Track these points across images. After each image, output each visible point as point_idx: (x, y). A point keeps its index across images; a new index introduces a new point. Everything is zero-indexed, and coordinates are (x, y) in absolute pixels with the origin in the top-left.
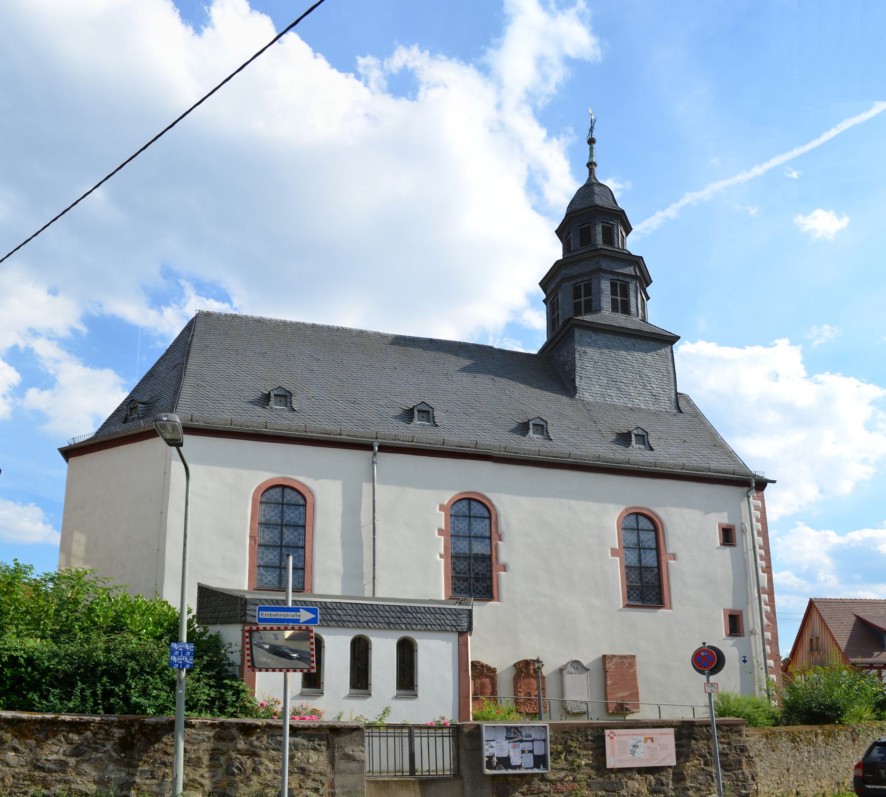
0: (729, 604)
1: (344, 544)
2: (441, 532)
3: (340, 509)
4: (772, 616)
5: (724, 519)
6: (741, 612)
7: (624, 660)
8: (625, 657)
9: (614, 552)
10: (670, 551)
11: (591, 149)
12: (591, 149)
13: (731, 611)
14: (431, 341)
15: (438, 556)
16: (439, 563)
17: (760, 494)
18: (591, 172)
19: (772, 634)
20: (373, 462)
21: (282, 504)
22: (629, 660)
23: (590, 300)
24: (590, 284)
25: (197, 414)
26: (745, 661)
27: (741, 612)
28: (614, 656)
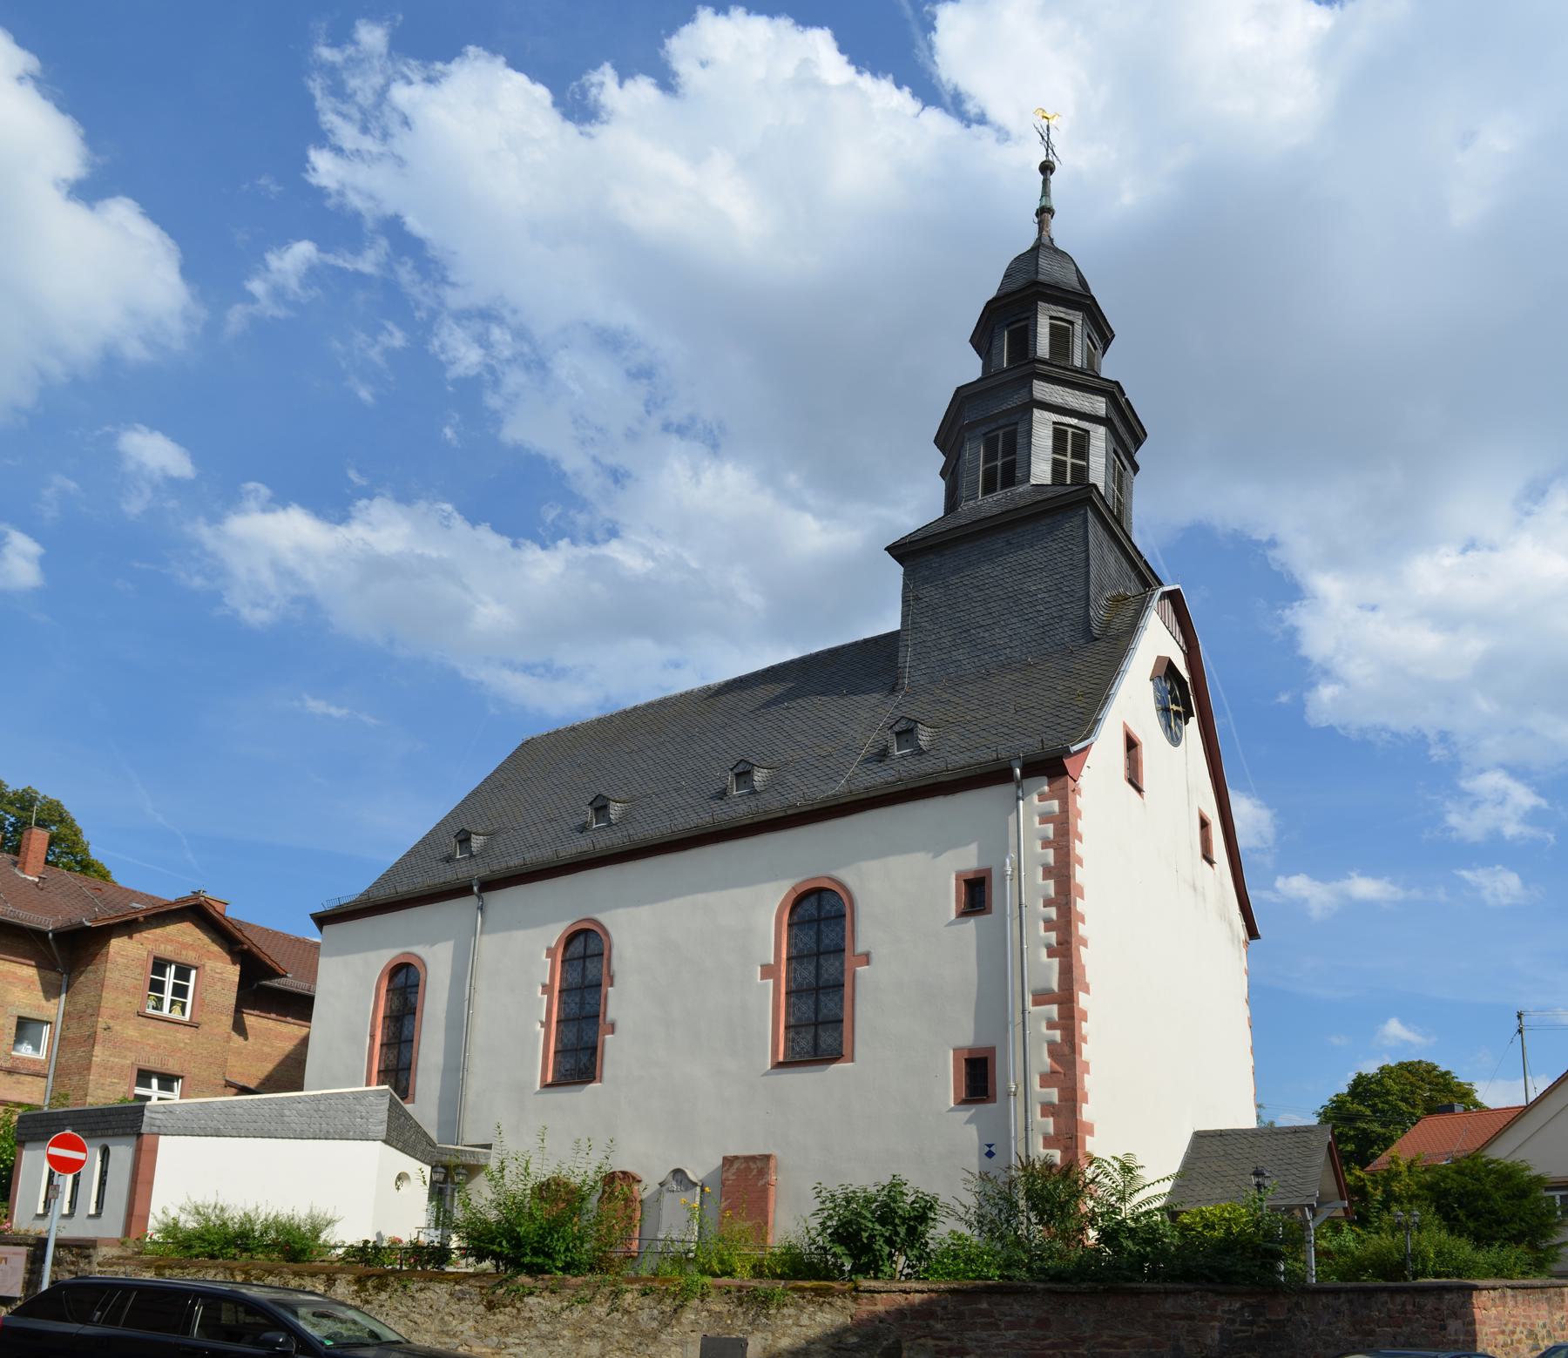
0: (966, 1036)
1: (448, 1028)
2: (547, 989)
3: (447, 982)
4: (1066, 1050)
5: (968, 859)
6: (992, 1050)
7: (752, 1165)
8: (753, 1158)
9: (768, 971)
10: (861, 948)
11: (1046, 183)
12: (1046, 183)
13: (970, 1050)
14: (735, 681)
15: (1044, 952)
16: (538, 1034)
17: (1058, 784)
18: (1042, 225)
19: (1061, 1091)
20: (1018, 799)
21: (819, 920)
22: (759, 1164)
23: (1013, 462)
24: (1015, 432)
25: (91, 976)
26: (990, 1154)
27: (992, 1050)
28: (736, 1158)
